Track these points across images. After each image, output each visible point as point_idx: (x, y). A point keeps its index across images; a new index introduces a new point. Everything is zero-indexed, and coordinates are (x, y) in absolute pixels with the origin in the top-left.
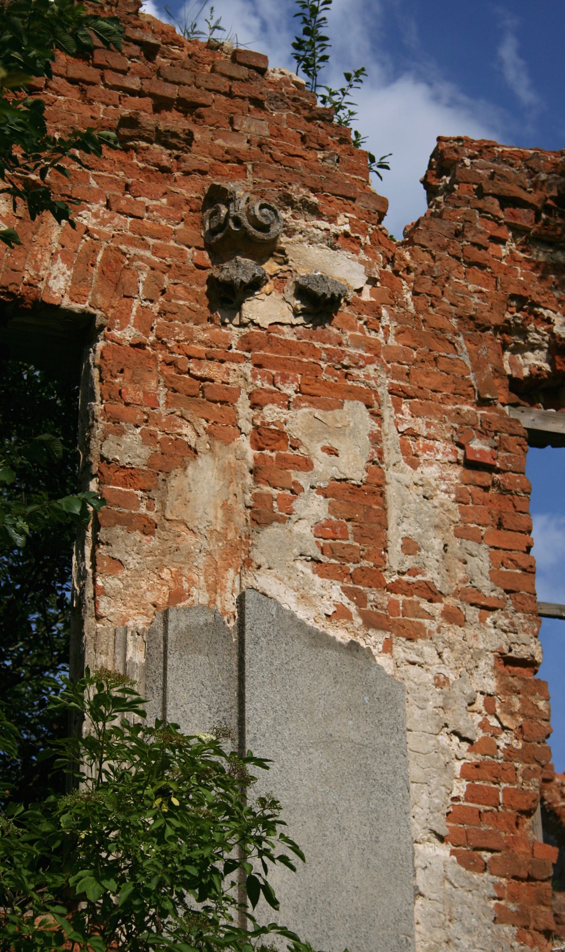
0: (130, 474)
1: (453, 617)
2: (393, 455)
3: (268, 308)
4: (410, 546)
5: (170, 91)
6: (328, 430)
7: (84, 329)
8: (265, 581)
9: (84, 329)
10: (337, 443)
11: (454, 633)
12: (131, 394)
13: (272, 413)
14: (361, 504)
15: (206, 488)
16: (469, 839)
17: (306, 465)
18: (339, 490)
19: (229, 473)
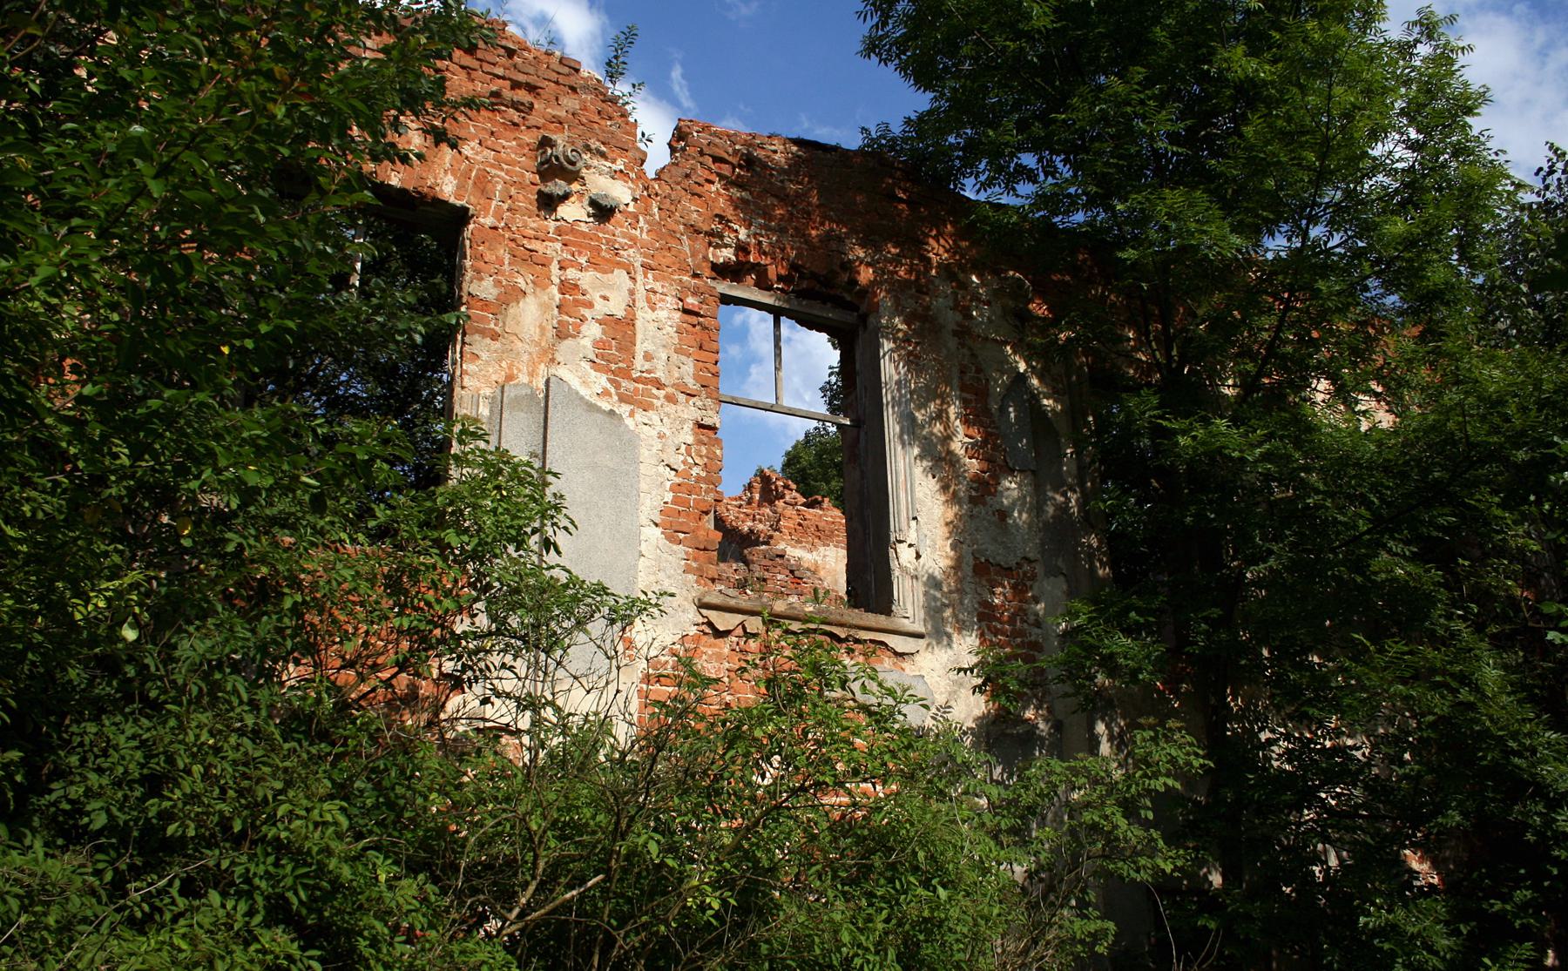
0: (485, 305)
1: (670, 399)
2: (641, 303)
3: (573, 211)
4: (648, 357)
5: (521, 78)
6: (605, 286)
7: (461, 217)
8: (562, 372)
9: (461, 217)
10: (609, 293)
11: (670, 408)
12: (489, 256)
13: (571, 273)
14: (621, 329)
15: (531, 315)
16: (673, 532)
17: (590, 305)
18: (609, 321)
19: (544, 307)
